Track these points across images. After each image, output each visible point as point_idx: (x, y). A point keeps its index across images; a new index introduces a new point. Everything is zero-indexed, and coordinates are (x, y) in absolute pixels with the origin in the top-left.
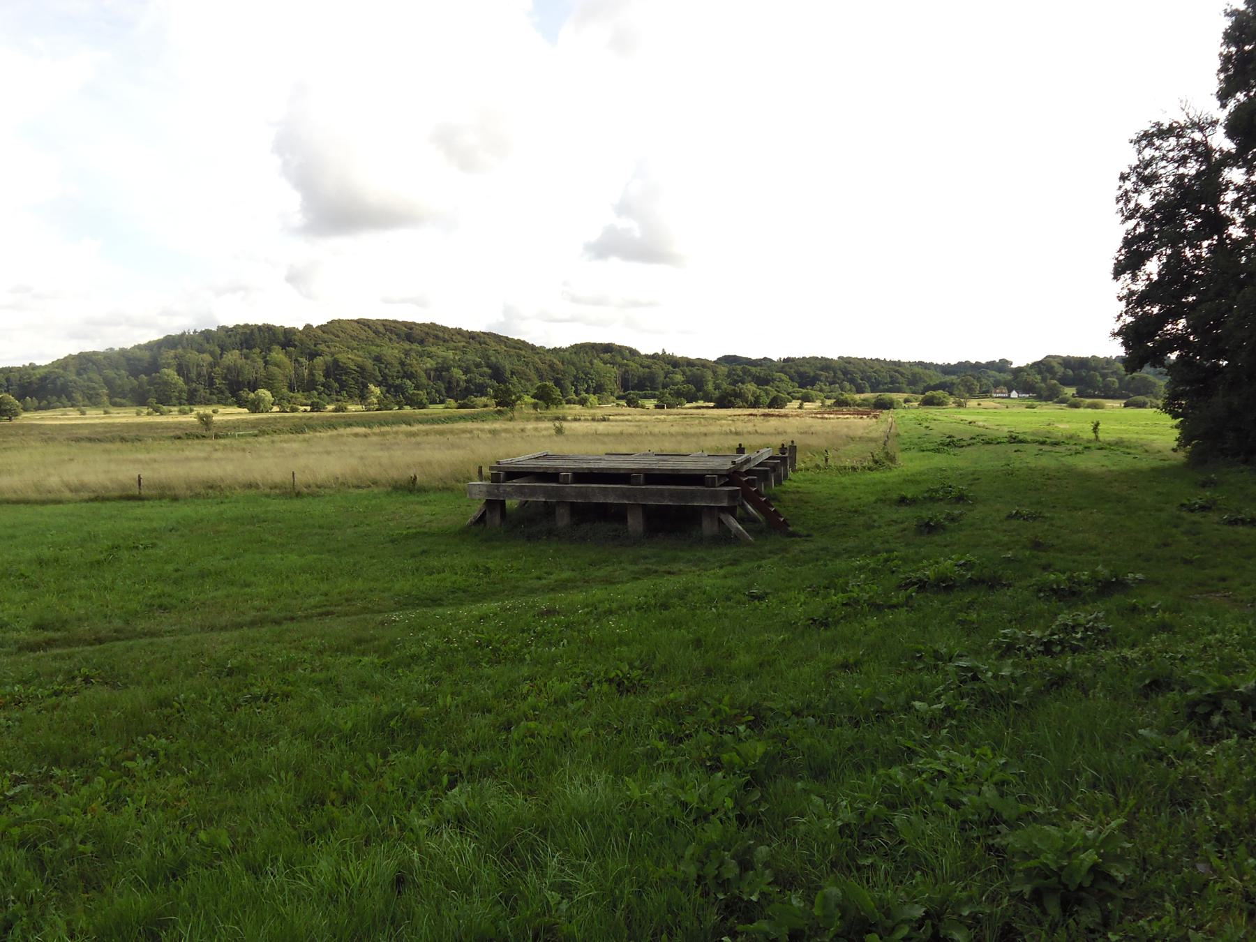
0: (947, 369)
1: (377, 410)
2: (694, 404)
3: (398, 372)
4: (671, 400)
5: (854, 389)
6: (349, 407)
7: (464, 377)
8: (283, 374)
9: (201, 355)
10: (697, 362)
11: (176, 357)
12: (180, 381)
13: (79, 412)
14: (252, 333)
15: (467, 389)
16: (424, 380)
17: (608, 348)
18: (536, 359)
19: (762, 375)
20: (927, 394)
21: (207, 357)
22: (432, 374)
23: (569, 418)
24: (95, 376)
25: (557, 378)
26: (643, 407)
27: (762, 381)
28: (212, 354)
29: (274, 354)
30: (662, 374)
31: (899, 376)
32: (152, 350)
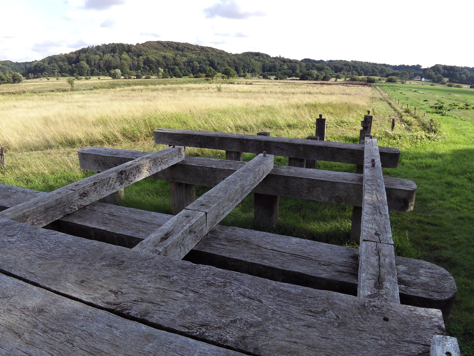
0: (395, 68)
1: (162, 78)
2: (291, 78)
3: (173, 63)
4: (282, 76)
5: (357, 74)
6: (152, 77)
7: (199, 65)
8: (127, 64)
9: (96, 56)
10: (294, 61)
11: (86, 57)
12: (88, 66)
13: (47, 79)
14: (115, 47)
15: (200, 70)
16: (183, 66)
17: (257, 54)
18: (228, 59)
19: (320, 67)
20: (389, 77)
21: (98, 57)
22: (186, 63)
23: (236, 83)
24: (55, 65)
25: (236, 66)
26: (270, 79)
27: (319, 69)
28: (100, 56)
29: (123, 55)
30: (279, 65)
31: (376, 69)
32: (77, 54)
